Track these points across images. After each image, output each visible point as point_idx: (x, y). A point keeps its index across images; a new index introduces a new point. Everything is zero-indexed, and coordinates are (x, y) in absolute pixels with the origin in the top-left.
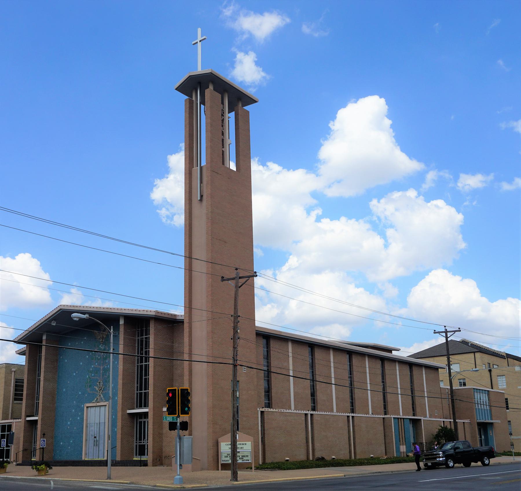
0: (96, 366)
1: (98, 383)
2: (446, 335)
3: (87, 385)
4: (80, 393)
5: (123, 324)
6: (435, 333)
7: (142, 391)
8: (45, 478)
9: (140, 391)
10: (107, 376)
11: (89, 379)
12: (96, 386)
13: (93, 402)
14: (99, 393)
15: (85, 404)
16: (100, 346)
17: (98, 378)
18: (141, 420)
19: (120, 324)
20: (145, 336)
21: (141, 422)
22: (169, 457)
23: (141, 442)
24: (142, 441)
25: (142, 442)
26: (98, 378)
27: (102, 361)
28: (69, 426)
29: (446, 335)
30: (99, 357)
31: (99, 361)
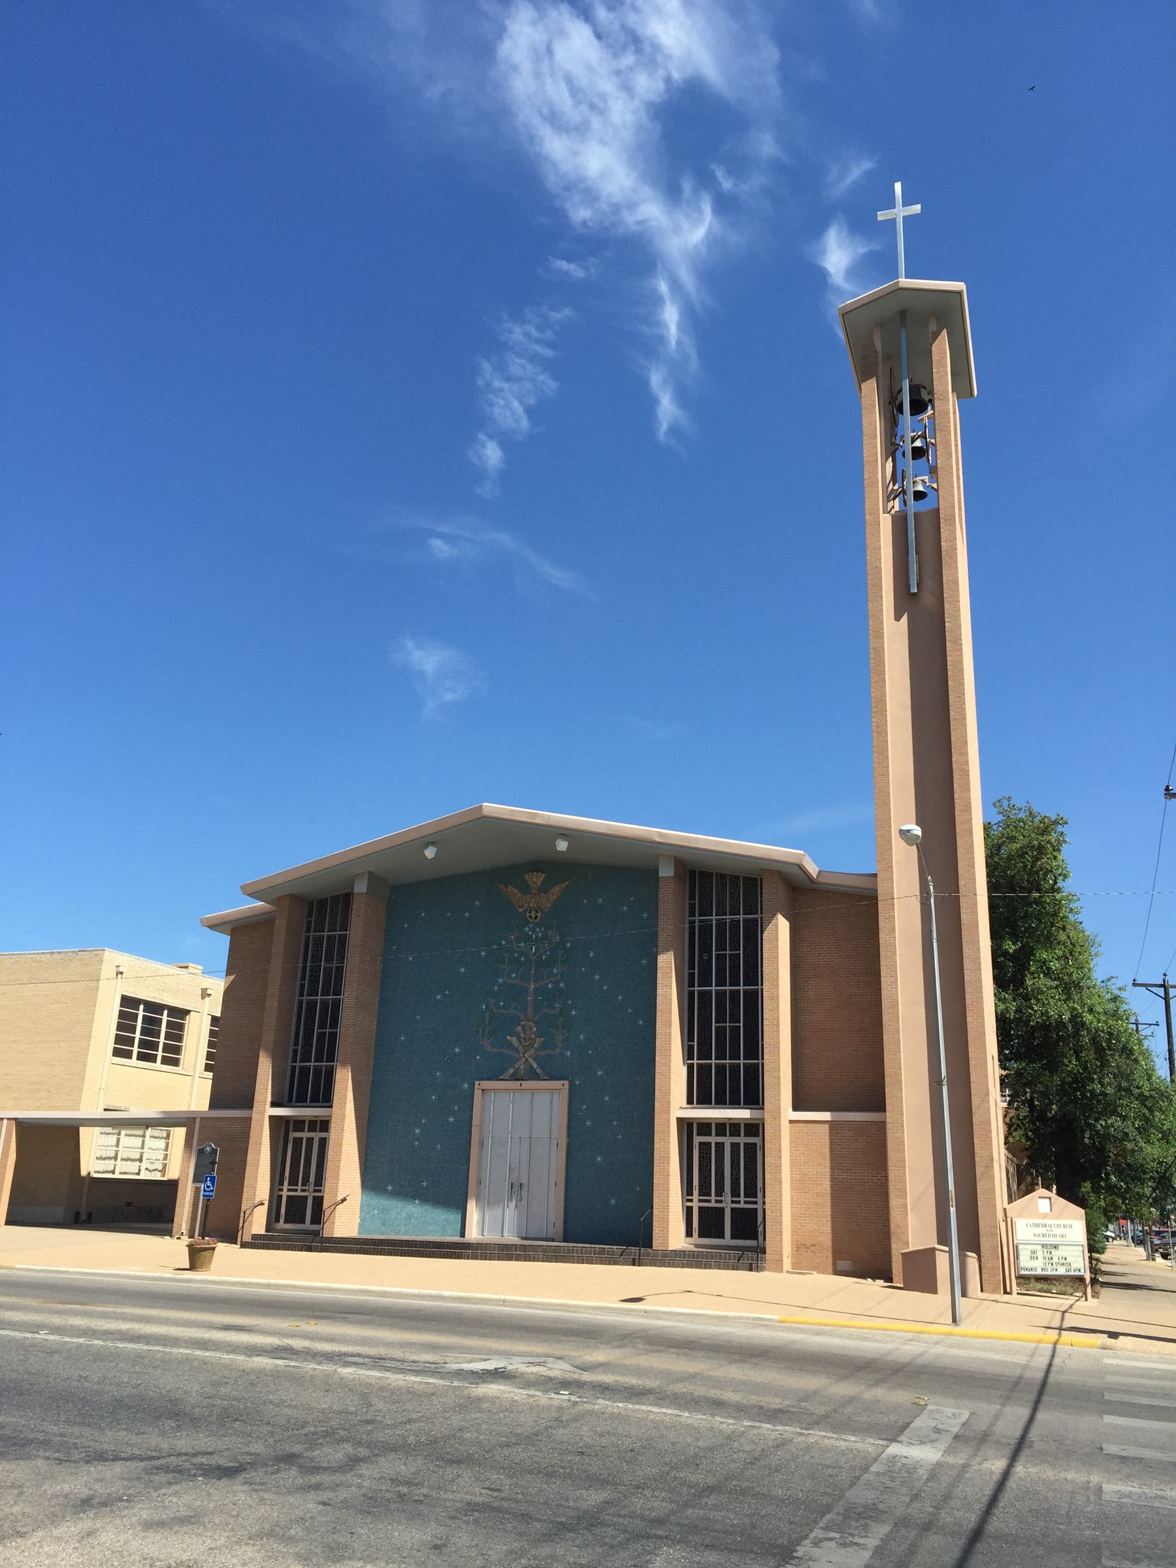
0: (510, 981)
1: (519, 1028)
2: (1166, 993)
3: (480, 1029)
4: (457, 1050)
5: (670, 877)
6: (1135, 985)
7: (311, 1062)
8: (520, 1310)
9: (302, 1061)
10: (558, 1010)
11: (487, 1014)
12: (511, 1035)
13: (501, 1077)
14: (522, 1055)
15: (477, 1083)
16: (527, 929)
17: (517, 1013)
18: (298, 1135)
19: (660, 875)
20: (328, 931)
21: (297, 1142)
22: (813, 1248)
23: (739, 1202)
24: (299, 1187)
25: (299, 1190)
26: (517, 1013)
27: (534, 969)
28: (418, 1139)
29: (1166, 993)
30: (523, 959)
31: (521, 969)
